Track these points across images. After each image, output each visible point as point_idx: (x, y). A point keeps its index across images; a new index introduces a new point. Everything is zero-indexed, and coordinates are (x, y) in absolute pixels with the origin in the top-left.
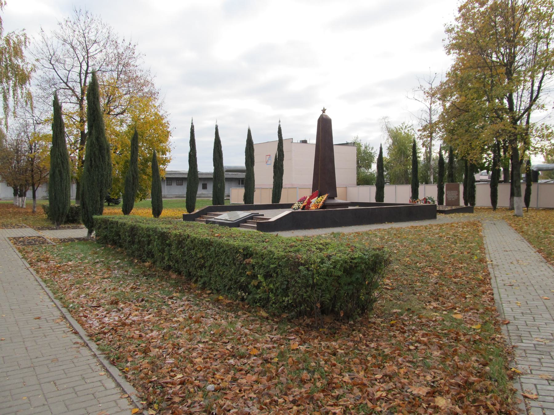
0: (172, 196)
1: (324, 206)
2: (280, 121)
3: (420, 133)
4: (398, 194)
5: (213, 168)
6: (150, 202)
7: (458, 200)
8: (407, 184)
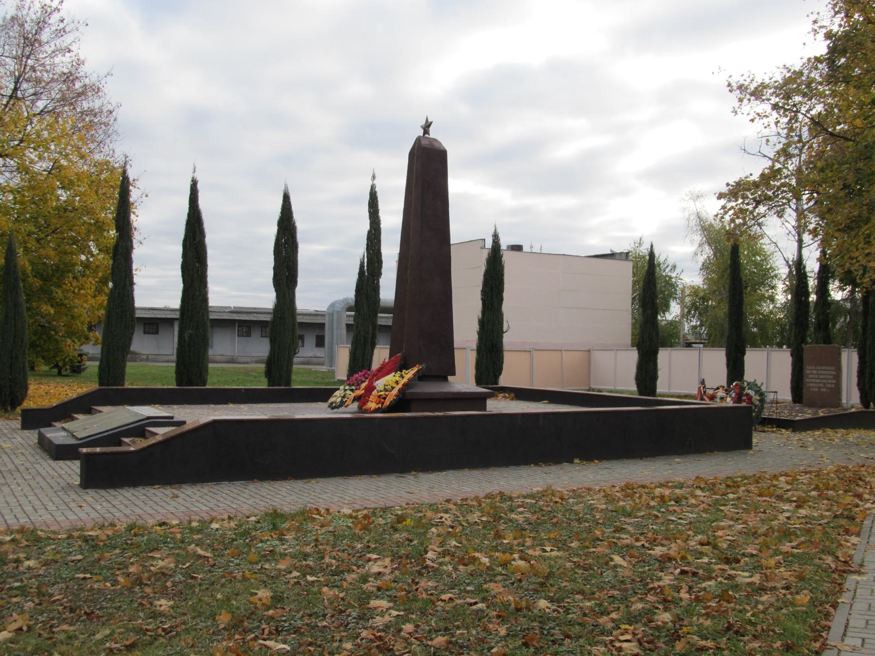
0: (249, 360)
1: (403, 402)
2: (374, 177)
3: (723, 202)
4: (690, 373)
5: (273, 295)
6: (96, 370)
7: (837, 390)
8: (720, 347)
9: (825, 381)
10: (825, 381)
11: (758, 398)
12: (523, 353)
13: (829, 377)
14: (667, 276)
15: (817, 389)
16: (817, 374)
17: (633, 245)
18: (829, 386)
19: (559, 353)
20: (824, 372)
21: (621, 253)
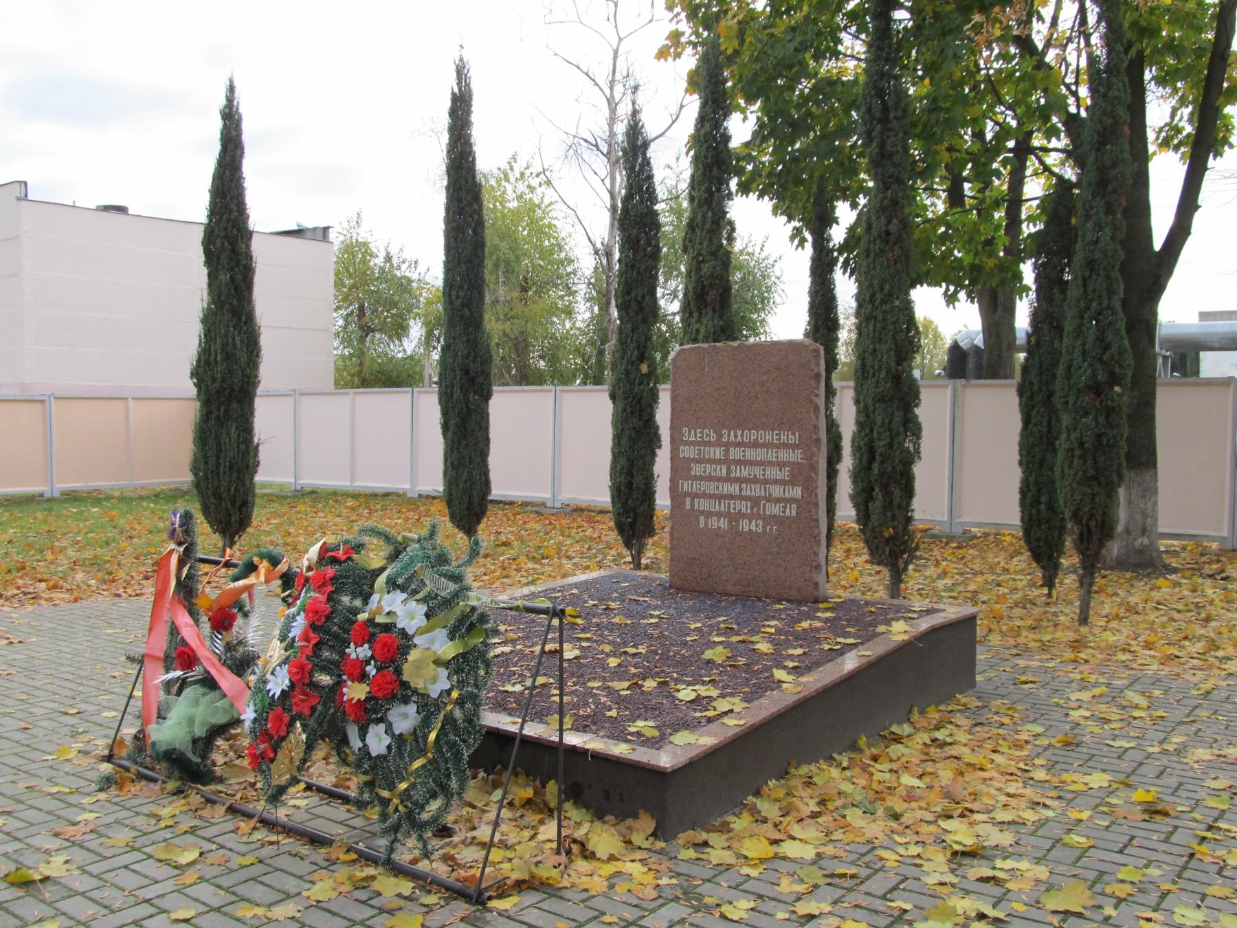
9: (758, 491)
10: (758, 491)
11: (448, 649)
12: (114, 403)
13: (773, 473)
14: (405, 277)
15: (723, 524)
16: (726, 461)
17: (345, 225)
18: (774, 510)
19: (121, 403)
20: (752, 454)
21: (315, 229)
